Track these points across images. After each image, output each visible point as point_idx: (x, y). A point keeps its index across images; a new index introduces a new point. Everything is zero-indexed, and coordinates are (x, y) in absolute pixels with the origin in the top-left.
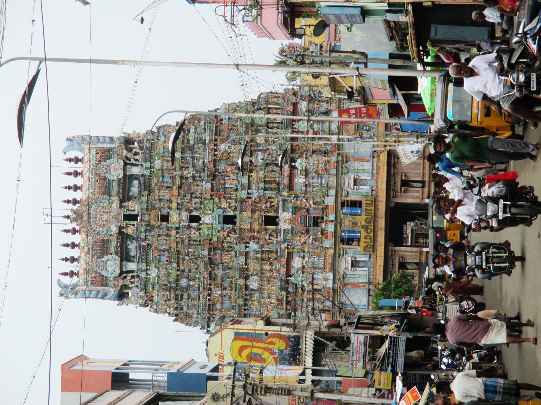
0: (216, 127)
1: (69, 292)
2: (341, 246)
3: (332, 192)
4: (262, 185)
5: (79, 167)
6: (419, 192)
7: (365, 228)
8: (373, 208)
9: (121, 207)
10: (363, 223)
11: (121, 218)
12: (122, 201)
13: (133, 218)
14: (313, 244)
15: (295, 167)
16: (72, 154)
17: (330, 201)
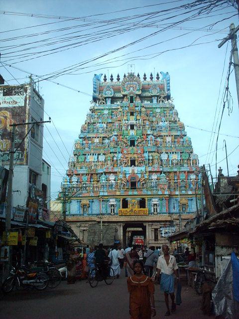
0: (179, 136)
1: (97, 78)
2: (122, 199)
3: (149, 193)
4: (151, 158)
5: (155, 79)
6: (152, 238)
7: (131, 210)
8: (142, 214)
9: (137, 95)
10: (134, 210)
11: (132, 95)
12: (139, 95)
13: (132, 101)
14: (122, 184)
15: (161, 173)
16: (160, 76)
17: (144, 192)
